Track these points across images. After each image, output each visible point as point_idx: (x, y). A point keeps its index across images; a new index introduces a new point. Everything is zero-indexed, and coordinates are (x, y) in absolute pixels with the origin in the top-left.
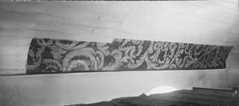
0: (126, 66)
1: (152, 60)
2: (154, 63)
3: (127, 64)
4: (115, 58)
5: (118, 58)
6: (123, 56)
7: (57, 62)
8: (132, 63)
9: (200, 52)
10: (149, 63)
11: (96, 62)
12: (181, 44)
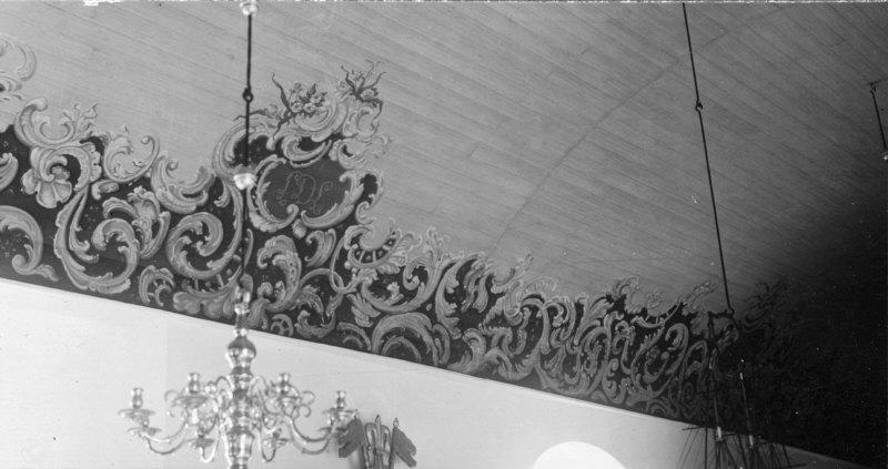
5: (478, 348)
6: (488, 347)
7: (362, 333)
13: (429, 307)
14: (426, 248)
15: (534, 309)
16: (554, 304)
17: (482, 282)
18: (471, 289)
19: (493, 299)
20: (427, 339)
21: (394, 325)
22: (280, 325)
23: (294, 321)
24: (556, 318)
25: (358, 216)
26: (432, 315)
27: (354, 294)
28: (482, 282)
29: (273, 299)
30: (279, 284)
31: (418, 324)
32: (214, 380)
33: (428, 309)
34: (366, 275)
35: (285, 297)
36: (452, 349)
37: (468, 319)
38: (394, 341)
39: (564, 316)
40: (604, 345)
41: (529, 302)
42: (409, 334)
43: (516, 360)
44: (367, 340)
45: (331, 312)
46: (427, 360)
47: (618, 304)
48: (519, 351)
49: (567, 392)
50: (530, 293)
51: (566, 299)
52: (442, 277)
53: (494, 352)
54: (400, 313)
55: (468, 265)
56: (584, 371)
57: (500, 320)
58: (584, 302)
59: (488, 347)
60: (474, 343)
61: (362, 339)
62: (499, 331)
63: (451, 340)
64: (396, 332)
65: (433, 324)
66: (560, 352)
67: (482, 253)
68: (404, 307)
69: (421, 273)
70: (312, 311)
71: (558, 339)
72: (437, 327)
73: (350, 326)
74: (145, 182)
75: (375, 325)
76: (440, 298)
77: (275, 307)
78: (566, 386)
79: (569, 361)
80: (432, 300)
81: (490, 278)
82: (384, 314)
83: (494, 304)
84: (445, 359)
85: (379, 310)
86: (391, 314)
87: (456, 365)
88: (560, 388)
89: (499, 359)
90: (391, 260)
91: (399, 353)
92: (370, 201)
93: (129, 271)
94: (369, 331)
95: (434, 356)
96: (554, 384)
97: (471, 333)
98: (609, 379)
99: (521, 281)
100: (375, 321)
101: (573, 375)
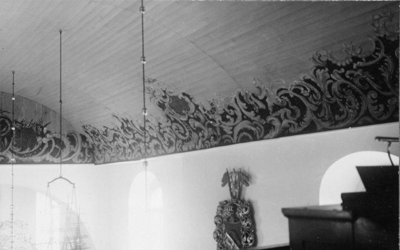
0: (287, 132)
1: (323, 117)
2: (326, 121)
3: (288, 128)
4: (275, 125)
5: (276, 123)
6: (281, 121)
7: (230, 137)
8: (294, 126)
9: (390, 88)
10: (319, 122)
11: (257, 132)
12: (75, 157)
13: (245, 117)
14: (222, 100)
15: (287, 95)
16: (293, 88)
17: (252, 98)
18: (252, 103)
19: (264, 101)
20: (253, 129)
21: (239, 129)
22: (206, 145)
23: (210, 141)
24: (302, 92)
25: (196, 103)
26: (248, 119)
27: (221, 124)
28: (252, 98)
29: (203, 137)
30: (203, 131)
31: (245, 124)
32: (72, 185)
33: (244, 118)
34: (218, 118)
35: (206, 134)
36: (265, 129)
37: (264, 113)
38: (241, 135)
39: (305, 89)
40: (350, 88)
41: (280, 94)
42: (245, 130)
43: (299, 120)
44: (232, 139)
45: (219, 134)
46: (255, 139)
47: (331, 66)
48: (298, 115)
49: (337, 126)
50: (276, 90)
51: (297, 82)
52: (238, 105)
53: (285, 122)
54: (238, 124)
55: (240, 95)
56: (350, 108)
57: (276, 108)
58: (308, 77)
59: (281, 121)
60: (273, 122)
61: (230, 139)
62: (281, 112)
63: (263, 125)
64: (241, 131)
65: (252, 122)
66: (325, 105)
67: (239, 90)
68: (237, 121)
69: (230, 107)
70: (214, 136)
71: (315, 100)
72: (254, 123)
73: (226, 136)
74: (160, 124)
75: (233, 132)
76: (370, 106)
77: (204, 139)
78: (336, 123)
79: (335, 108)
80: (243, 114)
81: (253, 95)
82: (234, 127)
83: (267, 103)
84: (262, 134)
85: (231, 126)
86: (235, 126)
87: (268, 136)
88: (331, 125)
89: (290, 124)
90: (219, 109)
91: (244, 140)
92: (192, 98)
93: (174, 144)
94: (232, 135)
95: (258, 135)
96: (326, 125)
97: (269, 119)
98: (374, 105)
99: (266, 88)
100: (232, 130)
101: (341, 114)
